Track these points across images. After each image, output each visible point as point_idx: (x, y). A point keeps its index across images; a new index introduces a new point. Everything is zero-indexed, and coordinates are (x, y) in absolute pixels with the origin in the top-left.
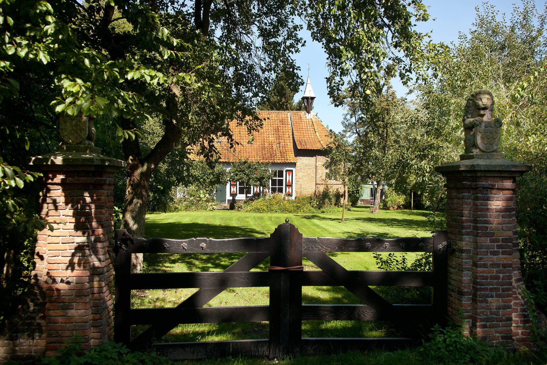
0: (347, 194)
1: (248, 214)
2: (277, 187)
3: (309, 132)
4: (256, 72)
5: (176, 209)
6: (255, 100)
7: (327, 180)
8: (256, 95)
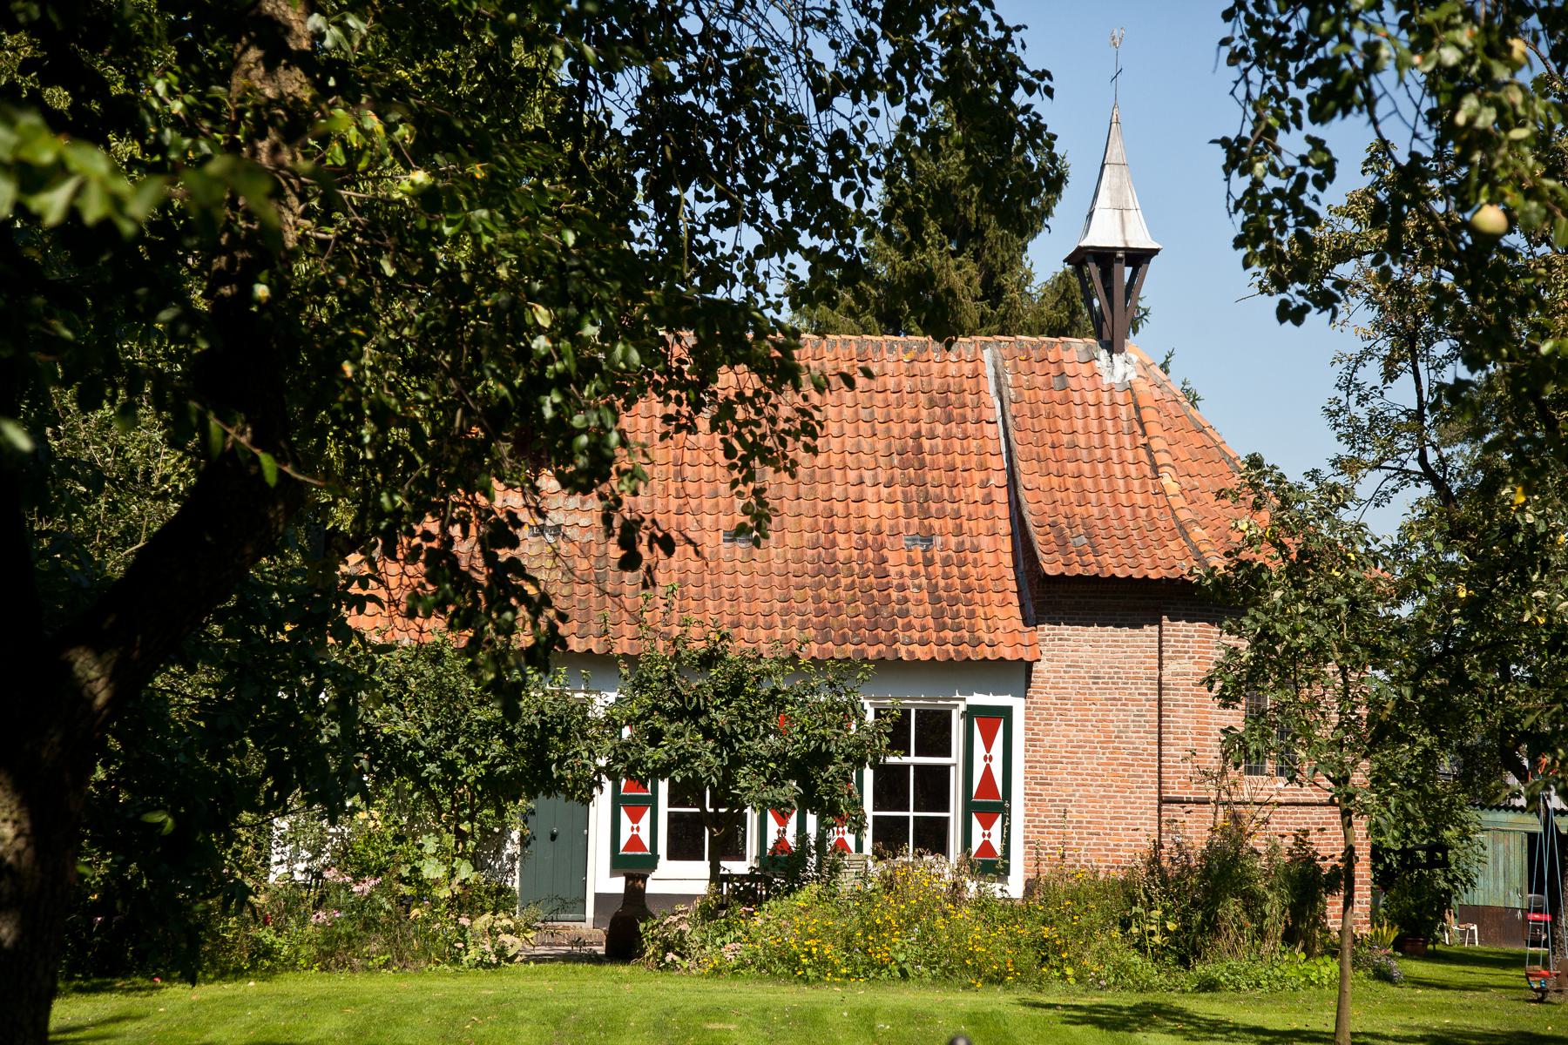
0: (1363, 872)
1: (723, 992)
2: (911, 814)
3: (1117, 469)
4: (780, 99)
5: (263, 961)
6: (776, 276)
7: (1233, 774)
8: (778, 242)
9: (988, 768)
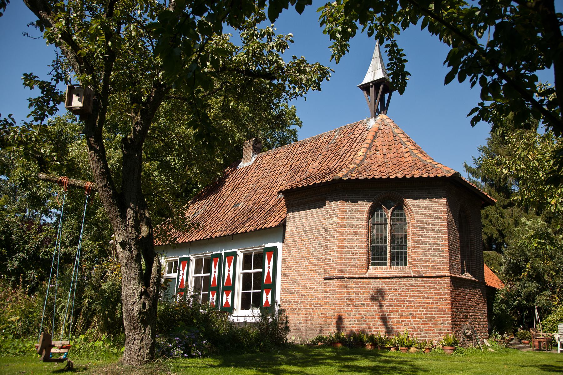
9: (229, 268)
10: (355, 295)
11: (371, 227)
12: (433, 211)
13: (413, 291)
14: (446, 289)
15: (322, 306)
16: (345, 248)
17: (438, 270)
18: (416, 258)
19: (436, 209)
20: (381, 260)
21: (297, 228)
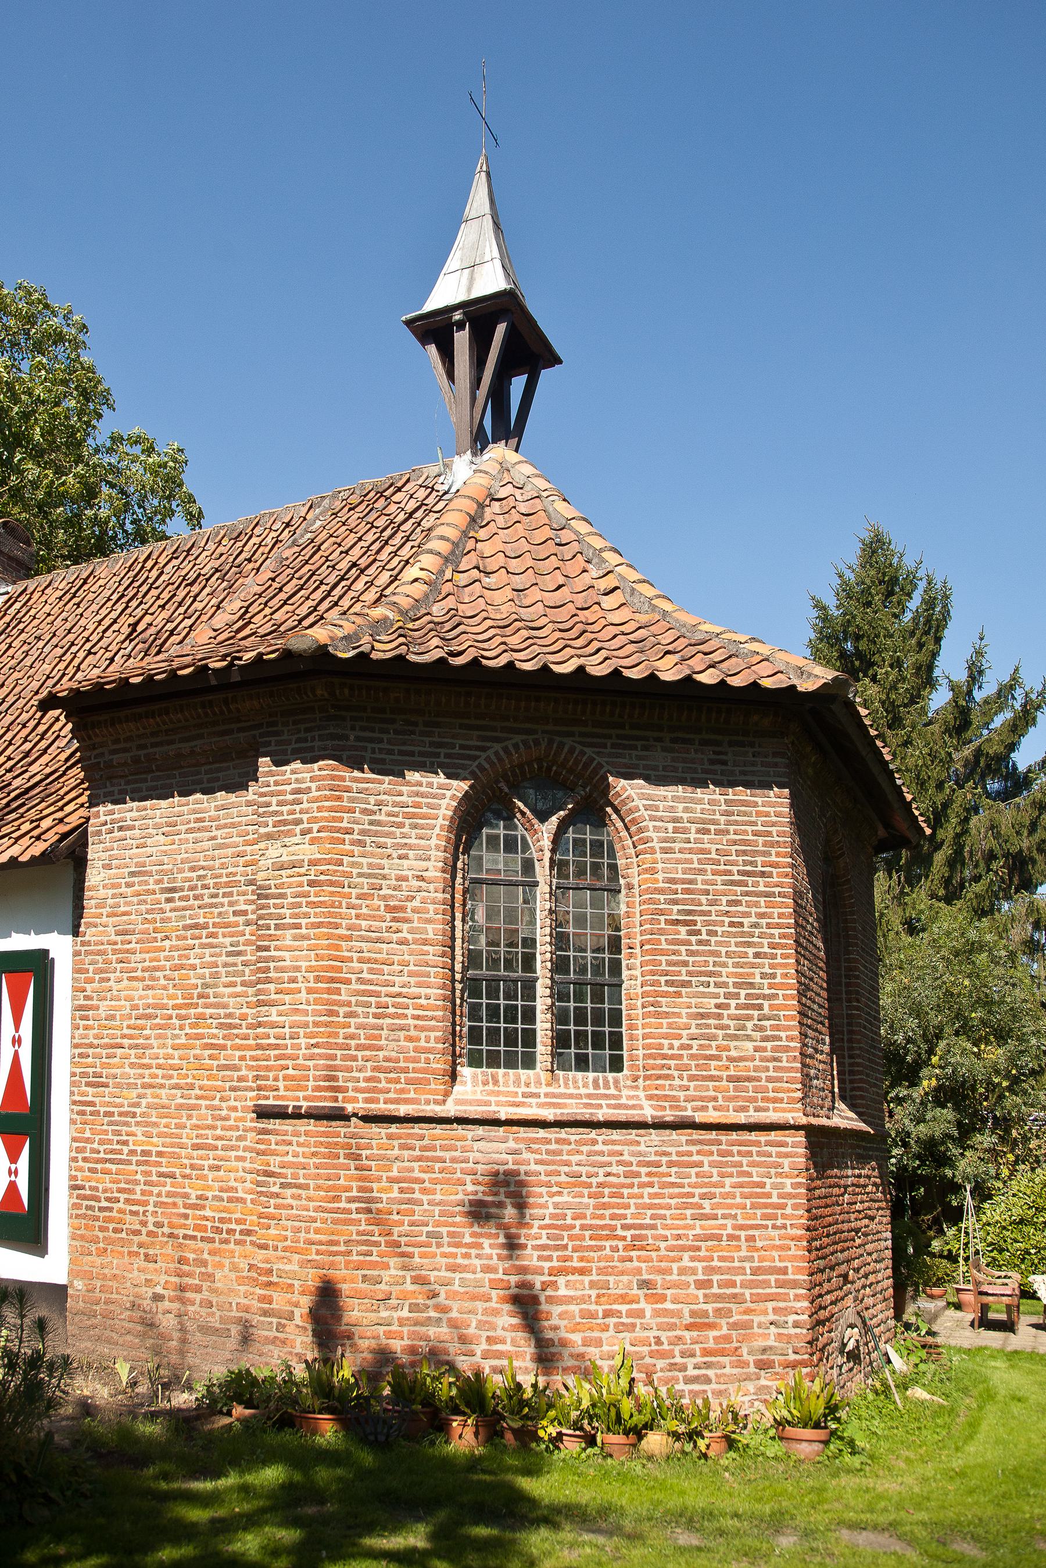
10: (395, 1194)
11: (465, 891)
12: (735, 843)
13: (651, 1185)
14: (788, 1182)
15: (249, 1233)
16: (348, 982)
17: (755, 1100)
18: (666, 1042)
19: (745, 832)
20: (511, 1041)
21: (132, 874)
